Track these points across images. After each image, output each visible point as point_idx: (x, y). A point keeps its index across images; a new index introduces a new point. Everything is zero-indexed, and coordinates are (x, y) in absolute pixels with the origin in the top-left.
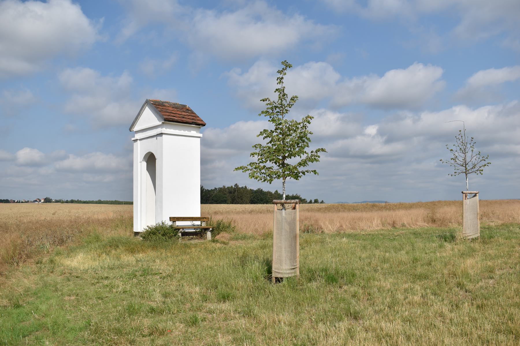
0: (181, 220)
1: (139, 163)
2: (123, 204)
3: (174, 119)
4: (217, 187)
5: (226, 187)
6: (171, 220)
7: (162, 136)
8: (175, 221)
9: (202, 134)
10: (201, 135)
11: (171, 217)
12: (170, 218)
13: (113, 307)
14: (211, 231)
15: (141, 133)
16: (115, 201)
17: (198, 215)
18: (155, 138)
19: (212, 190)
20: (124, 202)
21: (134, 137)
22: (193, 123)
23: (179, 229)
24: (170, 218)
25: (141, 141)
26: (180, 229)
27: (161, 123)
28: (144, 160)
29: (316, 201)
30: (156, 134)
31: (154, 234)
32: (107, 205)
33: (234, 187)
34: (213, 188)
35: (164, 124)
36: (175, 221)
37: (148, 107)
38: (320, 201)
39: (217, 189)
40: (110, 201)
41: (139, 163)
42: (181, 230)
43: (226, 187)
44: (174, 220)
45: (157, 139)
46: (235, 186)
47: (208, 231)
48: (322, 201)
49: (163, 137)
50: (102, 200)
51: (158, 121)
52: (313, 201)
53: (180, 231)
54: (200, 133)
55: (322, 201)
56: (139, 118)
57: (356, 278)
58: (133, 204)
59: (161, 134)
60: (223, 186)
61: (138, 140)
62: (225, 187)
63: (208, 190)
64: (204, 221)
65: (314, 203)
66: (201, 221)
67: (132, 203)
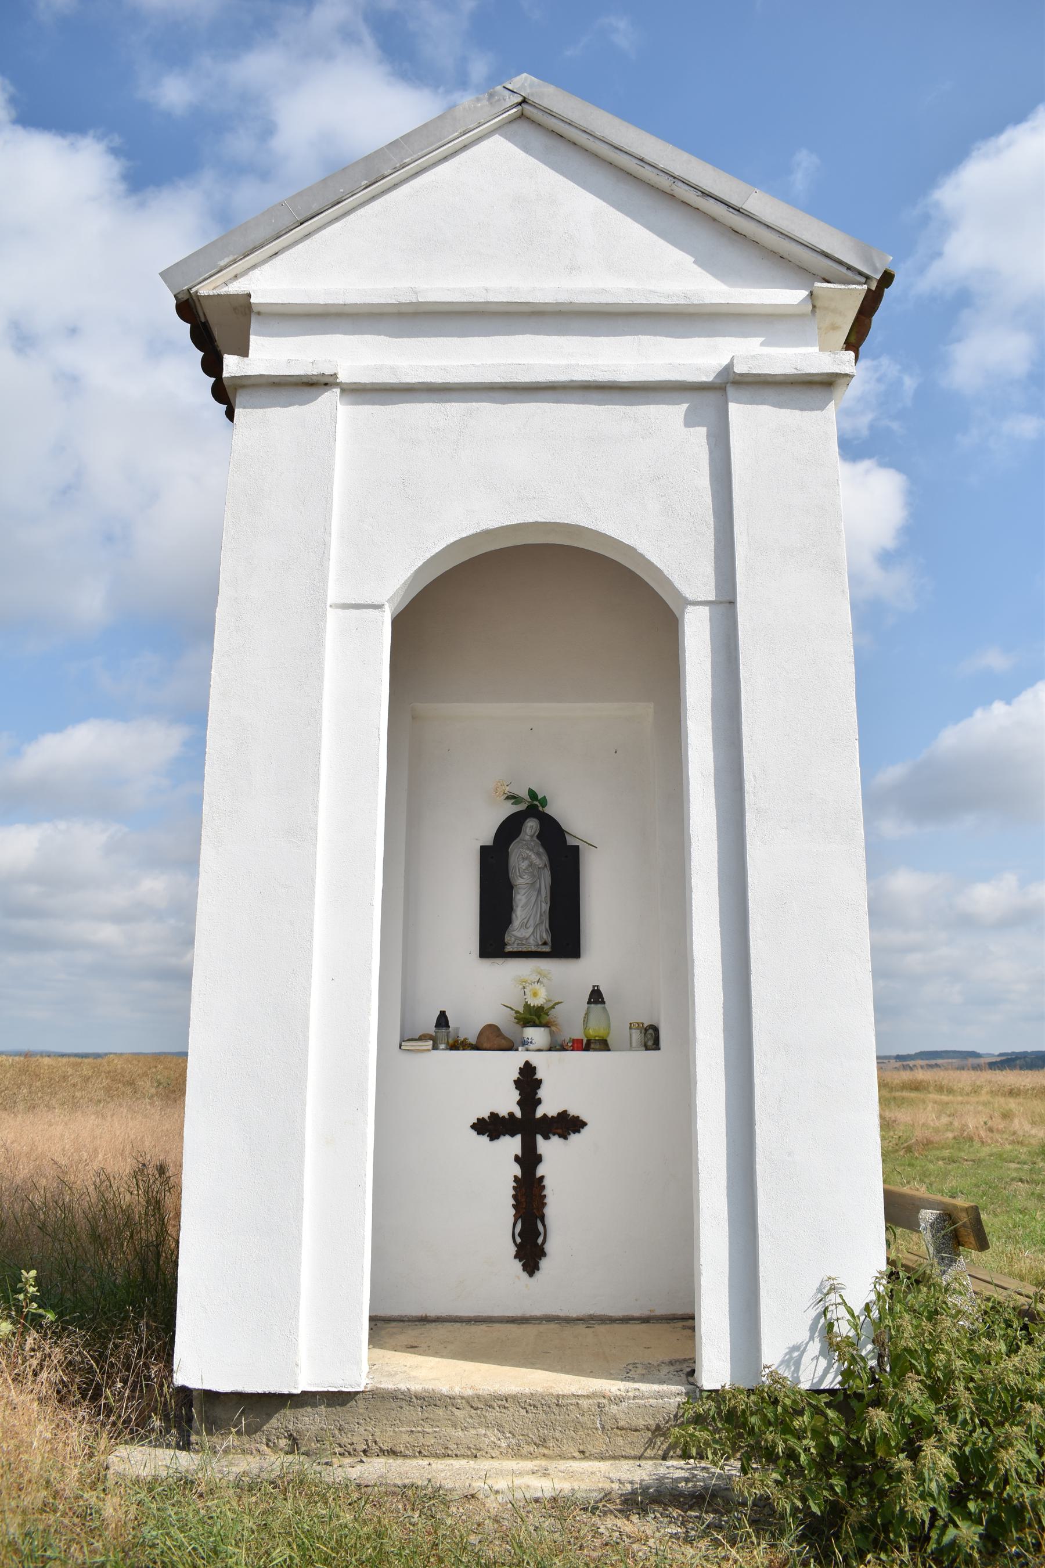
30: (708, 378)
61: (338, 391)
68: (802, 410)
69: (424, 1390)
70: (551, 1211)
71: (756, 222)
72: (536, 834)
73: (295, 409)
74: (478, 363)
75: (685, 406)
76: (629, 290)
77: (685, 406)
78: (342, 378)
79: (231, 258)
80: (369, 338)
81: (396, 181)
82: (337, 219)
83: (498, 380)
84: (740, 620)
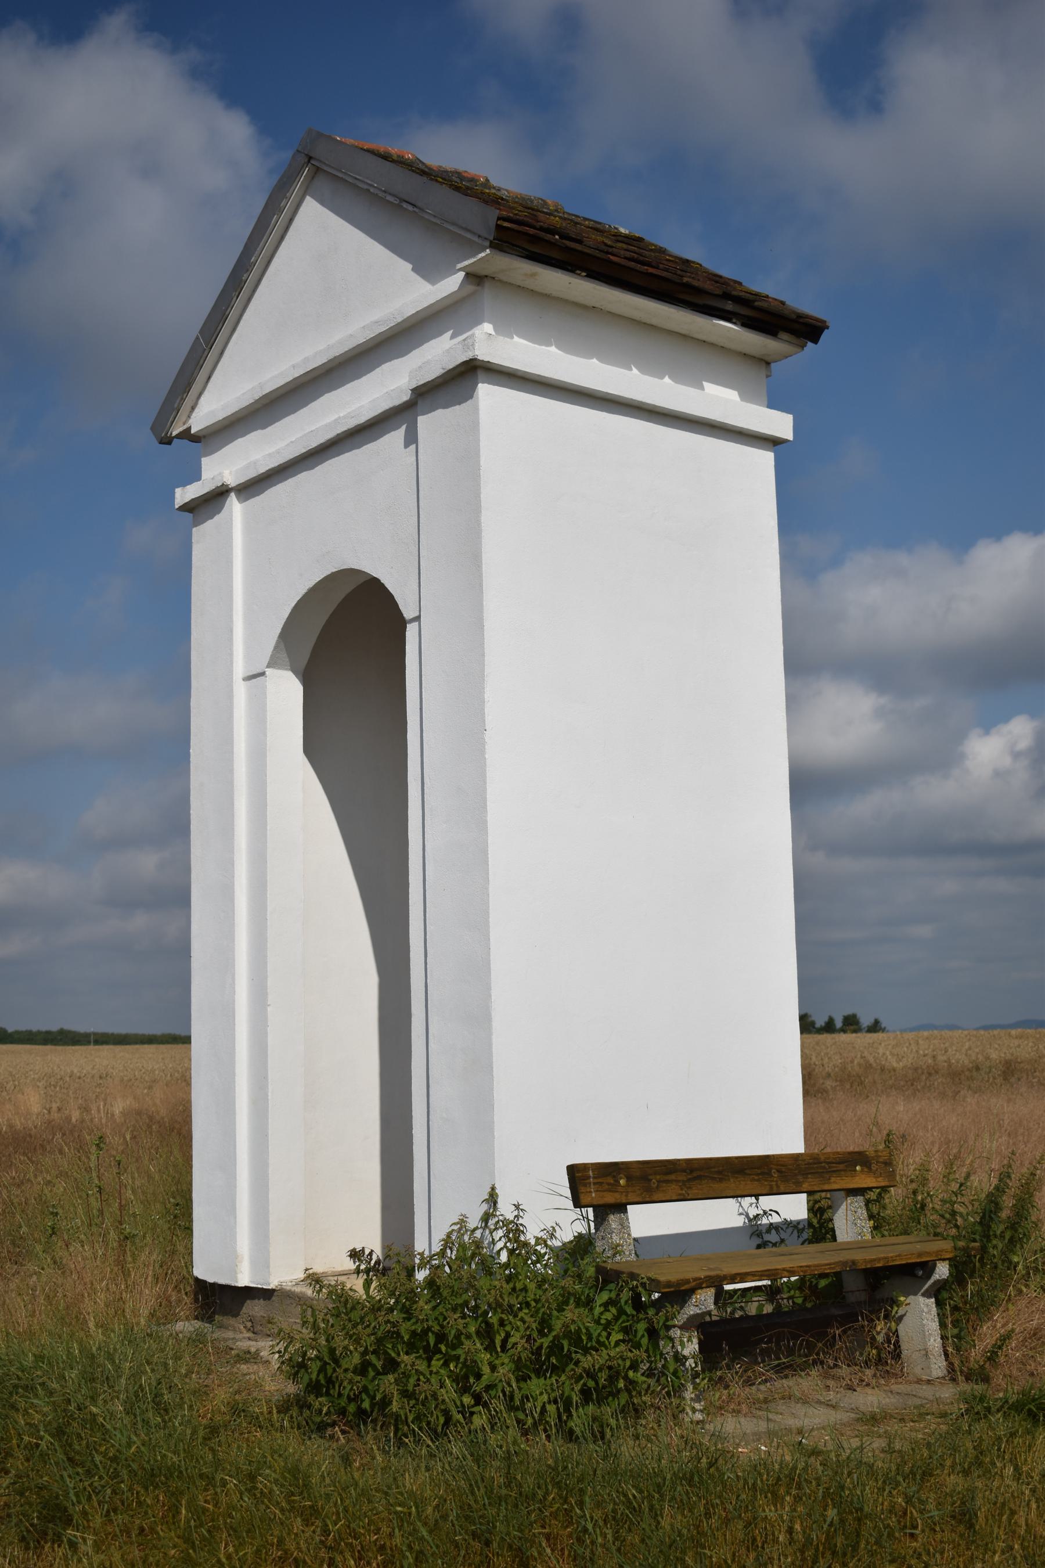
0: (674, 1189)
1: (241, 691)
2: (88, 1043)
3: (580, 242)
6: (584, 1199)
7: (469, 394)
9: (789, 418)
11: (584, 1167)
12: (577, 1175)
13: (69, 1173)
14: (938, 1292)
16: (62, 1032)
18: (396, 437)
20: (95, 1034)
21: (196, 476)
22: (729, 306)
23: (680, 1294)
24: (577, 1175)
26: (692, 1291)
27: (452, 283)
28: (284, 655)
29: (851, 1023)
30: (406, 397)
31: (430, 1354)
32: (28, 1047)
35: (487, 295)
36: (621, 1208)
37: (322, 202)
38: (866, 1021)
40: (39, 1032)
41: (241, 691)
42: (704, 1301)
44: (610, 1198)
45: (411, 439)
47: (915, 1294)
48: (877, 1022)
49: (476, 409)
50: (10, 1030)
52: (839, 1024)
53: (691, 1309)
54: (771, 405)
55: (877, 1022)
56: (233, 314)
58: (190, 1043)
61: (233, 495)
65: (843, 1030)
66: (810, 1193)
67: (187, 1040)
68: (460, 404)
69: (301, 1293)
73: (217, 518)
75: (404, 427)
77: (404, 427)
78: (231, 481)
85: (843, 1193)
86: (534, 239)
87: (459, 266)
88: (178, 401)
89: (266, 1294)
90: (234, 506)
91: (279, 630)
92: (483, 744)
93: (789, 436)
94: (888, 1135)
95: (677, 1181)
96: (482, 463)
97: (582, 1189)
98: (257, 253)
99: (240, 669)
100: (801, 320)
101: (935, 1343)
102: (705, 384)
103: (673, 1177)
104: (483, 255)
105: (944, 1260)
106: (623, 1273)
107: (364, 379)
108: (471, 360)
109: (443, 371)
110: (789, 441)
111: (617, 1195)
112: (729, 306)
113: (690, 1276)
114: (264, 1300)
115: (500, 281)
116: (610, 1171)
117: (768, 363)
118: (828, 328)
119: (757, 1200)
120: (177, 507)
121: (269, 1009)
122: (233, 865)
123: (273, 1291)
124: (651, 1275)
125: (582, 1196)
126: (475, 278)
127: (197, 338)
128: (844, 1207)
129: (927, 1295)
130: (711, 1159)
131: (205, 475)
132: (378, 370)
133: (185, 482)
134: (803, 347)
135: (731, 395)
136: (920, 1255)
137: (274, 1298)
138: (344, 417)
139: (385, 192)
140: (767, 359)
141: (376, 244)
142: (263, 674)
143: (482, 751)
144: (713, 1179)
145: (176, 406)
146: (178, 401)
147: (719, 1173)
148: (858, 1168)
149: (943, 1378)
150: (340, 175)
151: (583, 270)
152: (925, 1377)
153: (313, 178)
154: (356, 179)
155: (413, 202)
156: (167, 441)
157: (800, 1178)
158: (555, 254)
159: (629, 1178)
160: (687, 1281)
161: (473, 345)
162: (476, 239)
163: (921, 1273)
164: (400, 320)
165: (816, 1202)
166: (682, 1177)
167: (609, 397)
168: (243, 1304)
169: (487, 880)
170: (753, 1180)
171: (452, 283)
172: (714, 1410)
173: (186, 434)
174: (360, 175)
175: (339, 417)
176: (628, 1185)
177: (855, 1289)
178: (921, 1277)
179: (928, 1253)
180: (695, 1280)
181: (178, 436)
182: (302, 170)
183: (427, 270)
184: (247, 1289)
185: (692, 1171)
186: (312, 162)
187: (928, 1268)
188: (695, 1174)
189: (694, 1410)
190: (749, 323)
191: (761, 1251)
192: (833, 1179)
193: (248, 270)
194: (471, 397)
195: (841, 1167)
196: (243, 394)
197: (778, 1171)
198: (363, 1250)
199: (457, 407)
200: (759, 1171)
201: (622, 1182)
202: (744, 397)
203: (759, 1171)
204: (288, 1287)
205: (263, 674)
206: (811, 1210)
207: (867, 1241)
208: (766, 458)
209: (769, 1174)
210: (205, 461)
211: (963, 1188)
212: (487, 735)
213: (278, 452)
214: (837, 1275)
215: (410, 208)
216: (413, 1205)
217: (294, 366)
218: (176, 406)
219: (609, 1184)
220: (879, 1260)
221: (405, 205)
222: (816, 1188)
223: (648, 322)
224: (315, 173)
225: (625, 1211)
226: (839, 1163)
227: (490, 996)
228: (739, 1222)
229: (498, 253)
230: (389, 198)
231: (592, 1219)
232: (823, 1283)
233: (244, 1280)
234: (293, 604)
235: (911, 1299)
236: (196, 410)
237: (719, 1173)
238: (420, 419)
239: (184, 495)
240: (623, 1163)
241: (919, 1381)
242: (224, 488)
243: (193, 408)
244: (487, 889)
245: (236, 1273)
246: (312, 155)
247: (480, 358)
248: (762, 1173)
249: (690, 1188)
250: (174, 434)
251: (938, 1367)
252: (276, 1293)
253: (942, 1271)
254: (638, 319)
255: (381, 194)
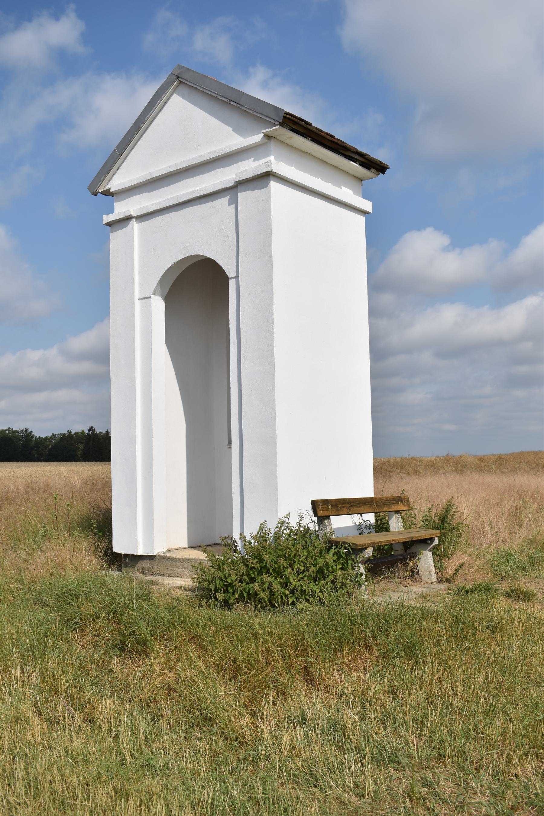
1: (138, 304)
4: (56, 433)
5: (73, 433)
7: (266, 185)
8: (327, 514)
10: (368, 206)
12: (314, 504)
15: (147, 193)
17: (369, 493)
18: (224, 201)
19: (47, 437)
21: (112, 211)
22: (356, 157)
24: (314, 504)
25: (147, 224)
26: (366, 548)
28: (159, 291)
30: (231, 184)
33: (87, 432)
34: (49, 435)
35: (273, 146)
36: (328, 517)
39: (57, 436)
41: (138, 304)
43: (73, 433)
46: (89, 431)
47: (425, 550)
51: (238, 134)
57: (100, 554)
59: (268, 176)
60: (69, 431)
61: (134, 220)
62: (71, 432)
63: (39, 438)
64: (397, 512)
66: (376, 513)
68: (260, 189)
69: (170, 556)
70: (303, 118)
71: (295, 146)
72: (232, 284)
73: (124, 229)
74: (169, 198)
75: (228, 197)
76: (208, 153)
77: (228, 197)
78: (134, 214)
79: (104, 176)
80: (144, 195)
81: (147, 126)
82: (133, 148)
83: (174, 203)
84: (155, 517)
85: (393, 513)
86: (295, 123)
87: (263, 131)
88: (103, 177)
89: (151, 558)
90: (134, 225)
91: (159, 279)
92: (273, 330)
93: (370, 210)
94: (403, 491)
95: (346, 507)
96: (272, 215)
97: (318, 510)
98: (148, 116)
99: (137, 295)
100: (381, 165)
101: (432, 569)
102: (342, 187)
103: (345, 505)
104: (276, 128)
105: (437, 537)
106: (339, 542)
107: (206, 175)
108: (269, 171)
109: (254, 175)
110: (370, 213)
111: (328, 512)
112: (356, 157)
113: (366, 542)
114: (149, 560)
115: (277, 139)
116: (326, 502)
117: (362, 181)
118: (389, 168)
119: (362, 516)
120: (104, 223)
121: (153, 439)
122: (135, 378)
123: (155, 556)
124: (353, 542)
125: (318, 513)
126: (268, 137)
127: (115, 150)
128: (394, 518)
129: (430, 551)
130: (356, 499)
131: (116, 211)
132: (214, 172)
133: (108, 213)
134: (378, 175)
135: (351, 192)
136: (431, 535)
137: (155, 559)
138: (197, 190)
139: (221, 96)
140: (362, 179)
141: (213, 118)
142: (150, 297)
143: (272, 334)
144: (357, 506)
145: (102, 179)
146: (103, 177)
147: (359, 504)
148: (399, 503)
149: (436, 582)
150: (196, 86)
151: (310, 137)
152: (429, 582)
153: (178, 86)
154: (205, 89)
155: (237, 102)
156: (95, 194)
157: (383, 506)
158: (301, 130)
159: (332, 506)
160: (365, 544)
161: (271, 165)
162: (272, 121)
163: (429, 542)
164: (228, 151)
165: (378, 517)
166: (348, 505)
167: (313, 190)
168: (137, 562)
169: (274, 386)
170: (369, 507)
171: (258, 138)
172: (374, 593)
173: (107, 193)
174: (212, 89)
175: (195, 190)
176: (331, 508)
177: (398, 551)
178: (429, 544)
179: (433, 534)
180: (368, 544)
181: (100, 193)
182: (174, 81)
183: (238, 130)
184: (142, 556)
185: (350, 503)
186: (179, 79)
187: (432, 540)
188: (351, 504)
189: (365, 594)
190: (362, 164)
191: (361, 535)
192: (392, 507)
193: (143, 123)
194: (266, 186)
195: (394, 502)
196: (141, 176)
197: (376, 504)
198: (226, 537)
199: (259, 191)
200: (370, 503)
201: (330, 507)
202: (354, 193)
203: (370, 503)
204: (162, 554)
205: (150, 297)
206: (376, 520)
207: (402, 531)
208: (362, 219)
209: (373, 504)
210: (116, 204)
211: (430, 510)
212: (275, 327)
213: (160, 203)
214: (391, 544)
215: (235, 104)
216: (232, 518)
217: (169, 167)
218: (102, 179)
219: (326, 508)
220: (419, 537)
221: (232, 103)
222: (378, 511)
223: (325, 160)
224: (179, 84)
225: (329, 518)
226: (394, 501)
227: (276, 433)
228: (351, 524)
229: (282, 128)
230: (223, 99)
231: (317, 522)
232: (386, 547)
233: (140, 552)
234: (167, 268)
235: (424, 552)
236: (111, 181)
237: (359, 504)
238: (239, 194)
239: (107, 218)
240: (329, 500)
241: (428, 583)
242: (130, 217)
243: (109, 181)
244: (274, 390)
245: (137, 549)
246: (179, 76)
247: (273, 171)
248: (371, 504)
249: (350, 510)
250: (100, 191)
251: (434, 578)
252: (156, 557)
253: (436, 541)
254: (321, 158)
255: (218, 97)
